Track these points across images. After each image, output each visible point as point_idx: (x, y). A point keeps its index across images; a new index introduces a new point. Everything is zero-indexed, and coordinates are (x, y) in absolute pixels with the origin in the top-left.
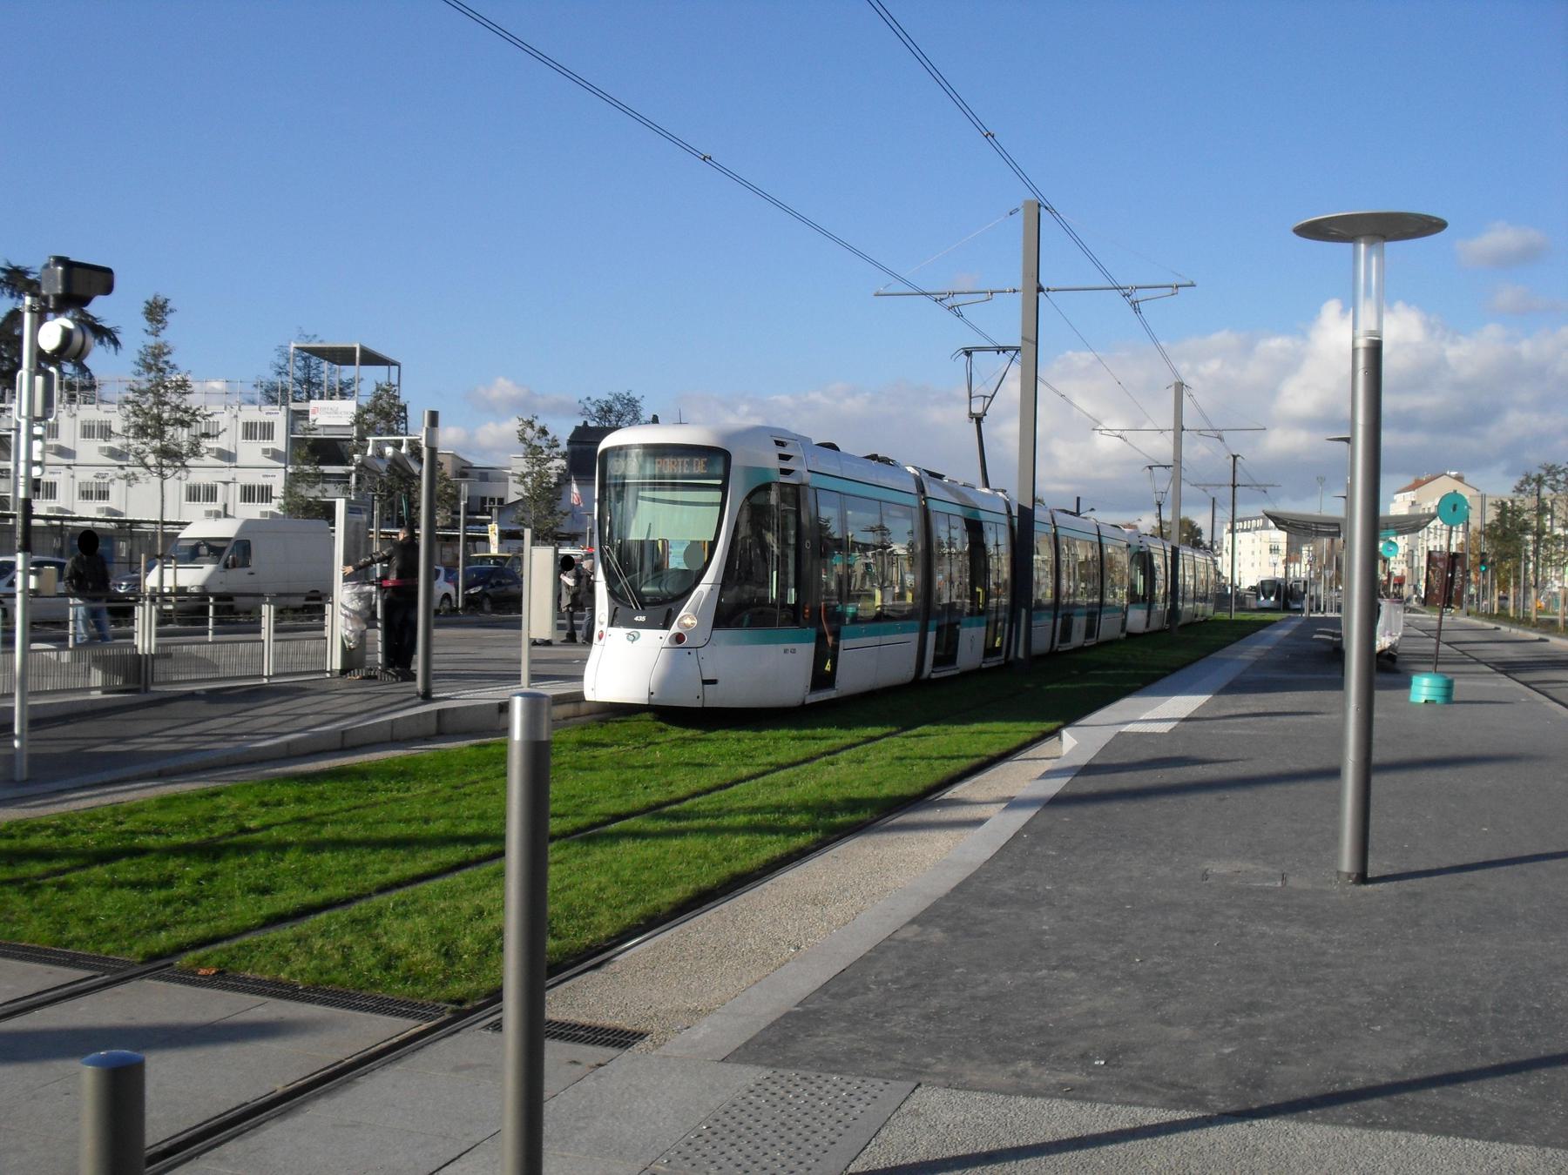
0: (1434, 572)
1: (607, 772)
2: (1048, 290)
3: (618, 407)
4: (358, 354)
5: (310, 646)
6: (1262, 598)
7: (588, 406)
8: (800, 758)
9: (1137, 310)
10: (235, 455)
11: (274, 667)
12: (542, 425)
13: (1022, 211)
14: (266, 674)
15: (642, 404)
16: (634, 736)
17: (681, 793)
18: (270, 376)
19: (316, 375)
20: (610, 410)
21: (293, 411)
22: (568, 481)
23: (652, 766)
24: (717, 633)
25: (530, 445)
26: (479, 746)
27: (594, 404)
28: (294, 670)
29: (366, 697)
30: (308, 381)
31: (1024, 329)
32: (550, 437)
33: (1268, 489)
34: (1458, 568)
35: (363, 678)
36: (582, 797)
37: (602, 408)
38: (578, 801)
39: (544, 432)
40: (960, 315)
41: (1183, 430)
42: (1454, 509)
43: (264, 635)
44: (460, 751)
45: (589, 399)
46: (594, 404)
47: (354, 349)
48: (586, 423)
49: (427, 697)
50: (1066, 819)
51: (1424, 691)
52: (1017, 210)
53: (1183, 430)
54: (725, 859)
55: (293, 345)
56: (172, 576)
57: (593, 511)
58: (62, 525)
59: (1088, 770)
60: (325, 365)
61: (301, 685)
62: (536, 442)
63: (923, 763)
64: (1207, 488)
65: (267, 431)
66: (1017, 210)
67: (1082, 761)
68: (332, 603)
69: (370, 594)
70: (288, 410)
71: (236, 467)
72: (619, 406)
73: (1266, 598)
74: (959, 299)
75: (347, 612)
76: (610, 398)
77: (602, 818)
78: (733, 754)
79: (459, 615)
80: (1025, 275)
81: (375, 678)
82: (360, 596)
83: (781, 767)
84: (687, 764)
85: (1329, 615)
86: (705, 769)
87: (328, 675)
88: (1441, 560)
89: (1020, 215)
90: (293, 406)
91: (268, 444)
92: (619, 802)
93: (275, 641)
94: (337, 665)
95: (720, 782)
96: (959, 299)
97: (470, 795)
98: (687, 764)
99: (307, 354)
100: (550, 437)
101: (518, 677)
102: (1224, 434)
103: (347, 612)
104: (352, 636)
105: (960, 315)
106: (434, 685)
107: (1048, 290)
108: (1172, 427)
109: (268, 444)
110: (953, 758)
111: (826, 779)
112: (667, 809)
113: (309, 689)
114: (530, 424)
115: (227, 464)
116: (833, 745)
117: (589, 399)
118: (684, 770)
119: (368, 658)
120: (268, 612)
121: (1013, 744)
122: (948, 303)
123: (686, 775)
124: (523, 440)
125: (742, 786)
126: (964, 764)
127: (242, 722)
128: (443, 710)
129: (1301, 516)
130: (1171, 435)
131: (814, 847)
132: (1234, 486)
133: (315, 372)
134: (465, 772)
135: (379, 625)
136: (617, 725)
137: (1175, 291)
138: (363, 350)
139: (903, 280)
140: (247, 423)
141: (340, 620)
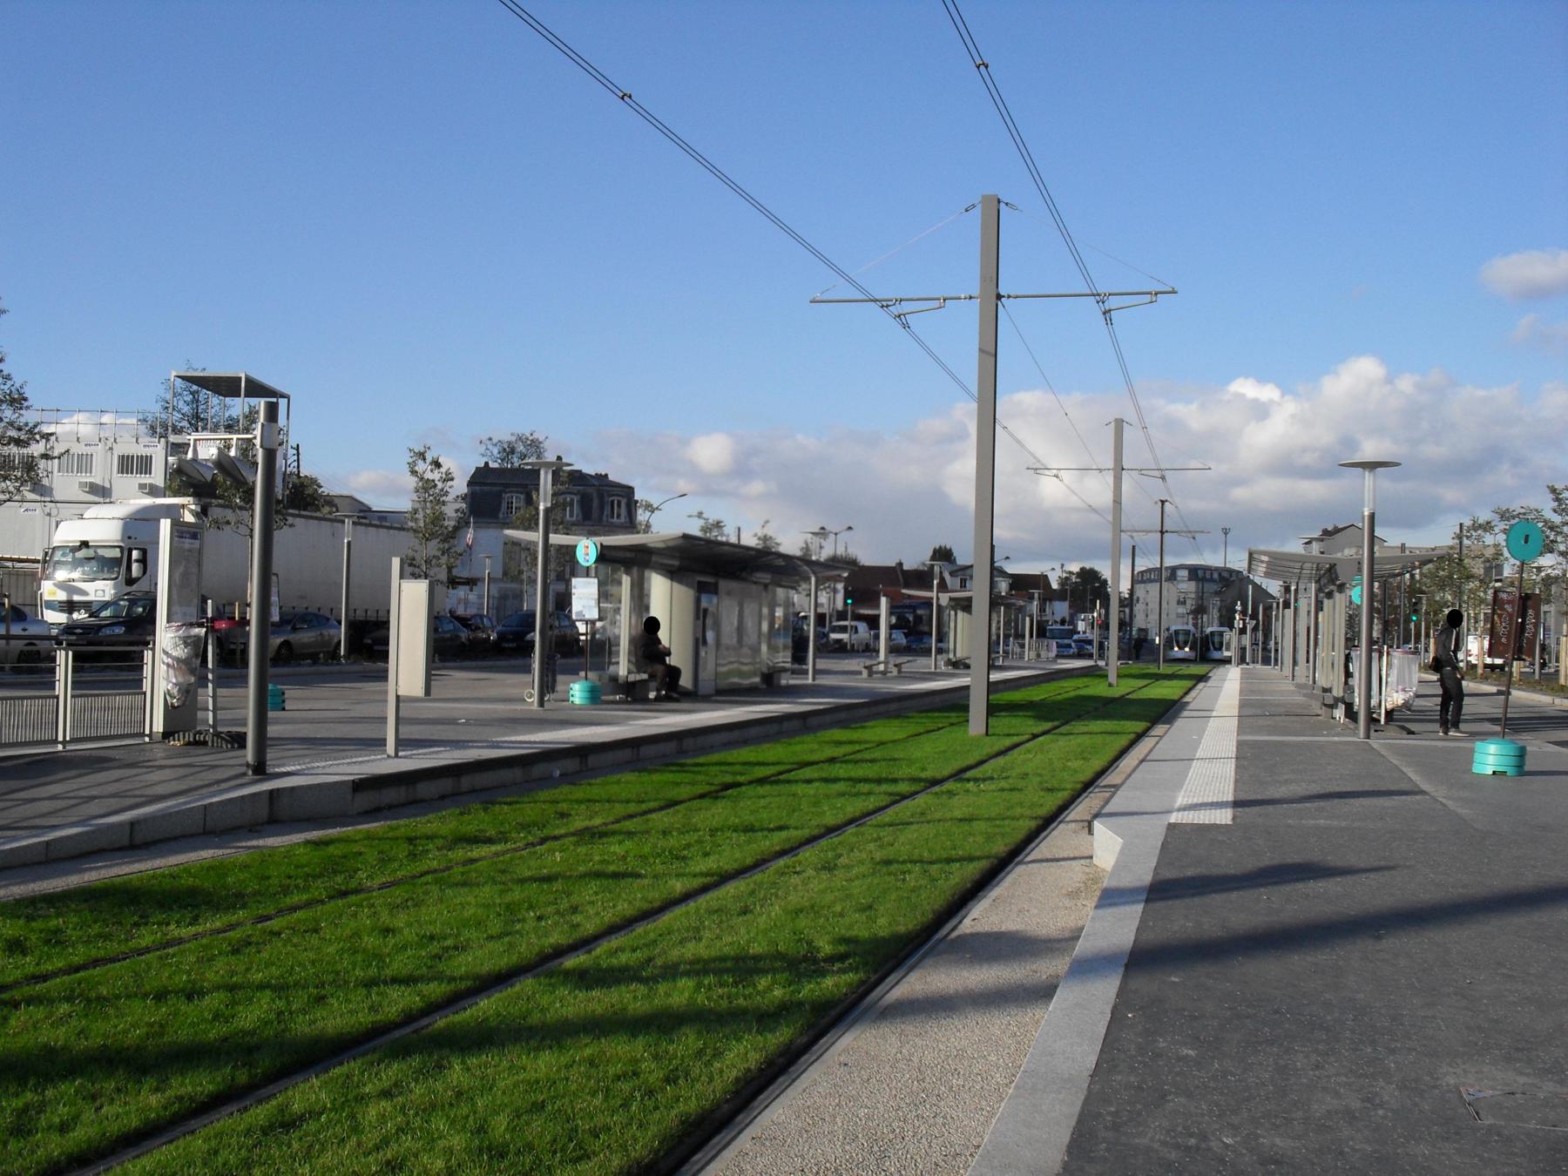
0: (1500, 616)
1: (487, 891)
2: (1009, 297)
3: (521, 448)
5: (121, 700)
6: (1176, 649)
7: (490, 447)
8: (749, 861)
10: (110, 490)
11: (72, 727)
12: (435, 456)
13: (979, 207)
14: (60, 738)
15: (546, 445)
16: (524, 827)
17: (590, 928)
18: (155, 409)
19: (205, 411)
20: (513, 451)
21: (173, 444)
22: (467, 524)
23: (548, 879)
25: (422, 479)
26: (317, 844)
27: (496, 445)
28: (101, 732)
29: (182, 771)
30: (197, 417)
33: (1197, 536)
34: (1530, 612)
35: (189, 744)
36: (445, 939)
37: (505, 449)
38: (434, 948)
39: (437, 465)
40: (906, 326)
41: (1123, 469)
43: (59, 689)
44: (289, 852)
45: (490, 439)
46: (496, 445)
47: (240, 378)
48: (487, 464)
51: (1491, 760)
52: (974, 206)
53: (1123, 469)
54: (668, 1080)
56: (1470, 698)
60: (215, 400)
61: (101, 753)
62: (429, 475)
63: (917, 868)
64: (1135, 534)
65: (144, 465)
66: (974, 206)
67: (1143, 874)
68: (153, 650)
69: (197, 637)
70: (167, 442)
72: (522, 448)
73: (1180, 648)
74: (906, 307)
75: (170, 661)
76: (514, 439)
77: (469, 983)
78: (659, 855)
79: (339, 664)
80: (983, 279)
81: (205, 743)
82: (186, 641)
83: (724, 878)
84: (598, 875)
86: (623, 883)
87: (147, 739)
88: (1509, 602)
89: (978, 211)
90: (173, 438)
91: (145, 479)
92: (497, 946)
93: (72, 696)
94: (159, 727)
95: (645, 906)
96: (906, 307)
97: (279, 934)
98: (598, 875)
99: (195, 387)
100: (443, 470)
101: (382, 742)
102: (1167, 474)
103: (170, 661)
104: (175, 691)
105: (906, 326)
106: (271, 754)
108: (1112, 466)
109: (145, 479)
111: (794, 899)
112: (570, 962)
113: (115, 760)
114: (422, 456)
115: (101, 500)
116: (788, 840)
117: (490, 439)
118: (594, 885)
119: (200, 714)
120: (63, 660)
121: (1019, 836)
122: (895, 310)
123: (596, 893)
125: (679, 911)
126: (973, 870)
127: (16, 806)
128: (278, 790)
130: (1110, 478)
131: (805, 1039)
132: (1162, 533)
133: (204, 407)
134: (286, 891)
135: (210, 676)
136: (506, 807)
138: (248, 380)
139: (851, 281)
140: (123, 456)
141: (161, 669)
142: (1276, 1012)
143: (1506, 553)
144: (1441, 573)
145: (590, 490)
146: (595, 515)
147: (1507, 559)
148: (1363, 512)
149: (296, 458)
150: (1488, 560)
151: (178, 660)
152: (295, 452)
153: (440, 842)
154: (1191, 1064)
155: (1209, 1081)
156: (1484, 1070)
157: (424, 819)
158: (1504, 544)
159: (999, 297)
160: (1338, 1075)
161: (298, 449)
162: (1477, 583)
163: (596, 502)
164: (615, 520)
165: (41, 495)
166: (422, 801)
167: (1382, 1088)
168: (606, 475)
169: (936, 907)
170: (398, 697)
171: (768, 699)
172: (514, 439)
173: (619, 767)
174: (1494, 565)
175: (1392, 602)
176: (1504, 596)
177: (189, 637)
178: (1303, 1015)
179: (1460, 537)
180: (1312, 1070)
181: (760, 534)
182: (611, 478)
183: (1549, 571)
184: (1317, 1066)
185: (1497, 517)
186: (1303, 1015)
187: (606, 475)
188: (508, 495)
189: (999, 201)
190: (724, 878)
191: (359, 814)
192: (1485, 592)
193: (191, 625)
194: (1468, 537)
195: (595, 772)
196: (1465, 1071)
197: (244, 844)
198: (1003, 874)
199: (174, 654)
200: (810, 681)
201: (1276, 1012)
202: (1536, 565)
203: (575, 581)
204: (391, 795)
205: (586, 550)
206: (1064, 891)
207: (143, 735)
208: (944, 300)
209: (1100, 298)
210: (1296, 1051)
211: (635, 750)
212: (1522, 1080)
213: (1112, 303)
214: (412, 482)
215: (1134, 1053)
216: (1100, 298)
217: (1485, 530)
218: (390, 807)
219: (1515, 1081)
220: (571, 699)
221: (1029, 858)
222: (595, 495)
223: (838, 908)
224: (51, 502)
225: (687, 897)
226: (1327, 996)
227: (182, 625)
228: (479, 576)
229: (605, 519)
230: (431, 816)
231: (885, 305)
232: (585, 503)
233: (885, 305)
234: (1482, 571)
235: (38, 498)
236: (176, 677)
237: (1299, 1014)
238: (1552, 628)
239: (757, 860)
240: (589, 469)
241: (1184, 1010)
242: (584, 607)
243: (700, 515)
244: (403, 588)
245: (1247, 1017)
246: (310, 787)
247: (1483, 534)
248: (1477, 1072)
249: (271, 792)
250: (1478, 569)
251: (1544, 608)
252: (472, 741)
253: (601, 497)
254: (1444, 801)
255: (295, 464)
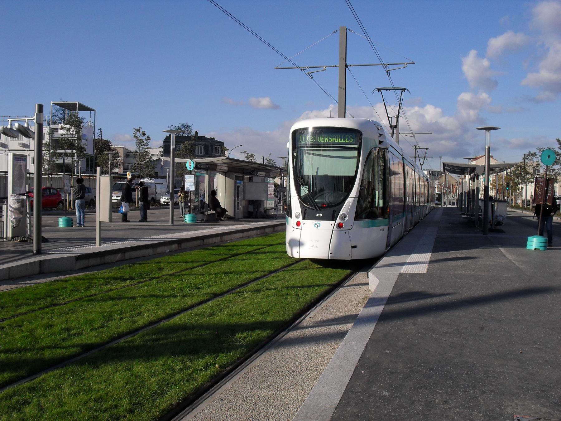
0: (538, 187)
2: (350, 66)
3: (183, 129)
4: (77, 106)
8: (225, 290)
9: (389, 75)
13: (339, 31)
15: (192, 128)
21: (52, 128)
24: (356, 222)
31: (340, 83)
32: (146, 136)
34: (550, 185)
39: (144, 134)
40: (312, 78)
41: (399, 134)
42: (549, 157)
45: (172, 126)
49: (39, 252)
50: (387, 351)
51: (534, 244)
53: (399, 134)
55: (52, 102)
57: (170, 167)
58: (30, 177)
59: (390, 300)
62: (141, 138)
66: (337, 31)
67: (386, 293)
68: (7, 204)
69: (23, 200)
70: (50, 128)
71: (30, 150)
74: (311, 70)
75: (12, 209)
76: (180, 125)
80: (341, 59)
82: (18, 201)
85: (448, 206)
88: (541, 182)
89: (338, 34)
90: (52, 126)
94: (10, 235)
95: (171, 312)
96: (311, 70)
100: (146, 136)
101: (94, 239)
102: (416, 135)
105: (312, 78)
107: (350, 66)
110: (310, 286)
114: (138, 131)
115: (26, 149)
117: (172, 126)
124: (136, 137)
126: (321, 290)
128: (43, 260)
129: (457, 164)
131: (209, 384)
132: (415, 158)
137: (406, 66)
138: (79, 104)
142: (431, 370)
143: (541, 164)
144: (517, 172)
145: (207, 143)
146: (210, 152)
147: (541, 166)
148: (485, 147)
149: (100, 133)
150: (534, 167)
151: (15, 209)
152: (100, 131)
153: (102, 281)
154: (385, 400)
155: (391, 412)
156: (526, 403)
157: (102, 271)
158: (540, 161)
159: (347, 66)
160: (455, 407)
161: (101, 130)
162: (530, 176)
163: (210, 148)
164: (217, 154)
165: (4, 148)
166: (108, 263)
167: (475, 415)
168: (214, 138)
169: (295, 312)
170: (100, 222)
171: (262, 220)
172: (180, 125)
173: (194, 248)
174: (536, 170)
175: (500, 182)
176: (540, 179)
177: (19, 199)
178: (443, 371)
179: (524, 159)
180: (443, 404)
181: (268, 159)
182: (215, 139)
183: (557, 171)
184: (446, 402)
185: (538, 151)
186: (443, 371)
187: (214, 138)
188: (178, 146)
189: (346, 29)
190: (215, 295)
191: (79, 269)
192: (533, 179)
193: (20, 195)
194: (527, 159)
195: (184, 250)
196: (517, 405)
197: (25, 282)
198: (330, 295)
199: (13, 206)
200: (282, 213)
201: (431, 370)
202: (552, 169)
203: (186, 176)
204: (93, 261)
205: (190, 164)
206: (353, 303)
207: (3, 238)
208: (326, 67)
209: (385, 66)
210: (437, 393)
211: (202, 241)
212: (544, 410)
213: (390, 68)
214: (135, 141)
215: (359, 394)
216: (385, 66)
217: (533, 156)
218: (93, 266)
219: (541, 411)
220: (185, 221)
221: (346, 285)
222: (210, 145)
223: (252, 313)
224: (8, 150)
225: (192, 307)
226: (456, 360)
227: (17, 195)
228: (165, 175)
229: (213, 154)
230: (106, 270)
231: (302, 69)
232: (206, 148)
233: (302, 69)
234: (532, 171)
235: (3, 149)
236: (14, 215)
237: (441, 371)
238: (558, 192)
239: (230, 289)
240: (208, 136)
241: (388, 369)
242: (189, 186)
243: (245, 152)
244: (101, 179)
245: (417, 373)
246: (57, 259)
247: (533, 157)
248: (522, 405)
249: (40, 261)
250: (531, 170)
251: (555, 185)
252: (140, 238)
253: (212, 146)
254: (514, 262)
255: (100, 135)
